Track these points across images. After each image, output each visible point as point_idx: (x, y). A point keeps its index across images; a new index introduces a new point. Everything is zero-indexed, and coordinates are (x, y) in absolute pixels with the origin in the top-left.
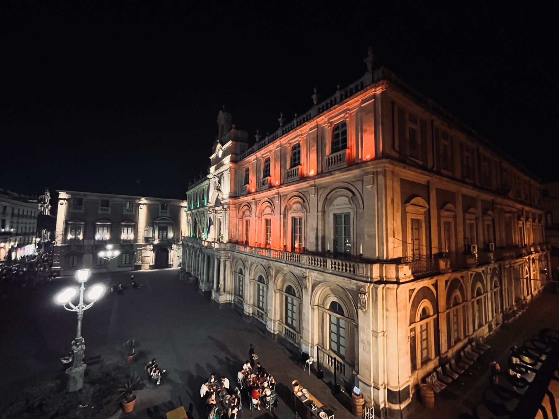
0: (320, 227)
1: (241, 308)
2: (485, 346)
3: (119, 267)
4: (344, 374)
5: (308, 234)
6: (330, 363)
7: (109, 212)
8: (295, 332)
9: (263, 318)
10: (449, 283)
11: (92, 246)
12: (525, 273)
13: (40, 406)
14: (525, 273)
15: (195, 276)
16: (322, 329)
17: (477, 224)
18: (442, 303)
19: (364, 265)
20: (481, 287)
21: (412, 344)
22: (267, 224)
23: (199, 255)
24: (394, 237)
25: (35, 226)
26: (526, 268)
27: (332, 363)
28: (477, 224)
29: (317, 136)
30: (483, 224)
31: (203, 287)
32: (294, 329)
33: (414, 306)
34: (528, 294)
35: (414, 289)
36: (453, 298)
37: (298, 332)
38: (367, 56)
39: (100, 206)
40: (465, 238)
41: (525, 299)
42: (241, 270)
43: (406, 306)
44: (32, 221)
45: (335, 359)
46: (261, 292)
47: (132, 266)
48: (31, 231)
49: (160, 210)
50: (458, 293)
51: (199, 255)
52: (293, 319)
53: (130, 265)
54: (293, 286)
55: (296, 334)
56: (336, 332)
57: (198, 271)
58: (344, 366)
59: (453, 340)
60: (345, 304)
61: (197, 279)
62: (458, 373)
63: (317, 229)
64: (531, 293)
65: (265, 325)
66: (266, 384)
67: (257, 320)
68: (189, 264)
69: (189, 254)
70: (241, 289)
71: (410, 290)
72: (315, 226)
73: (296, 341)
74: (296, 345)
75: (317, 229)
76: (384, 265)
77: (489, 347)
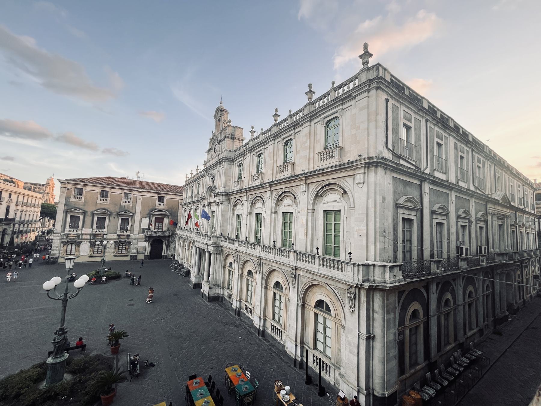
0: (310, 224)
1: (229, 302)
2: (476, 352)
4: (330, 376)
6: (315, 363)
7: (108, 202)
10: (440, 286)
11: (91, 235)
12: (517, 276)
13: (17, 396)
14: (517, 276)
17: (470, 226)
18: (433, 306)
19: (507, 251)
20: (473, 290)
24: (385, 236)
25: (39, 214)
26: (519, 272)
27: (317, 362)
28: (470, 226)
30: (476, 226)
31: (193, 279)
32: (281, 325)
33: (404, 309)
34: (520, 299)
35: (404, 291)
37: (284, 330)
41: (516, 303)
42: (231, 263)
43: (395, 308)
44: (36, 209)
45: (320, 359)
49: (157, 203)
50: (449, 296)
52: (280, 317)
53: (126, 254)
55: (283, 330)
58: (330, 367)
59: (443, 344)
64: (524, 298)
65: (252, 320)
69: (183, 247)
71: (217, 109)
72: (305, 223)
74: (282, 343)
76: (178, 232)
77: (480, 353)
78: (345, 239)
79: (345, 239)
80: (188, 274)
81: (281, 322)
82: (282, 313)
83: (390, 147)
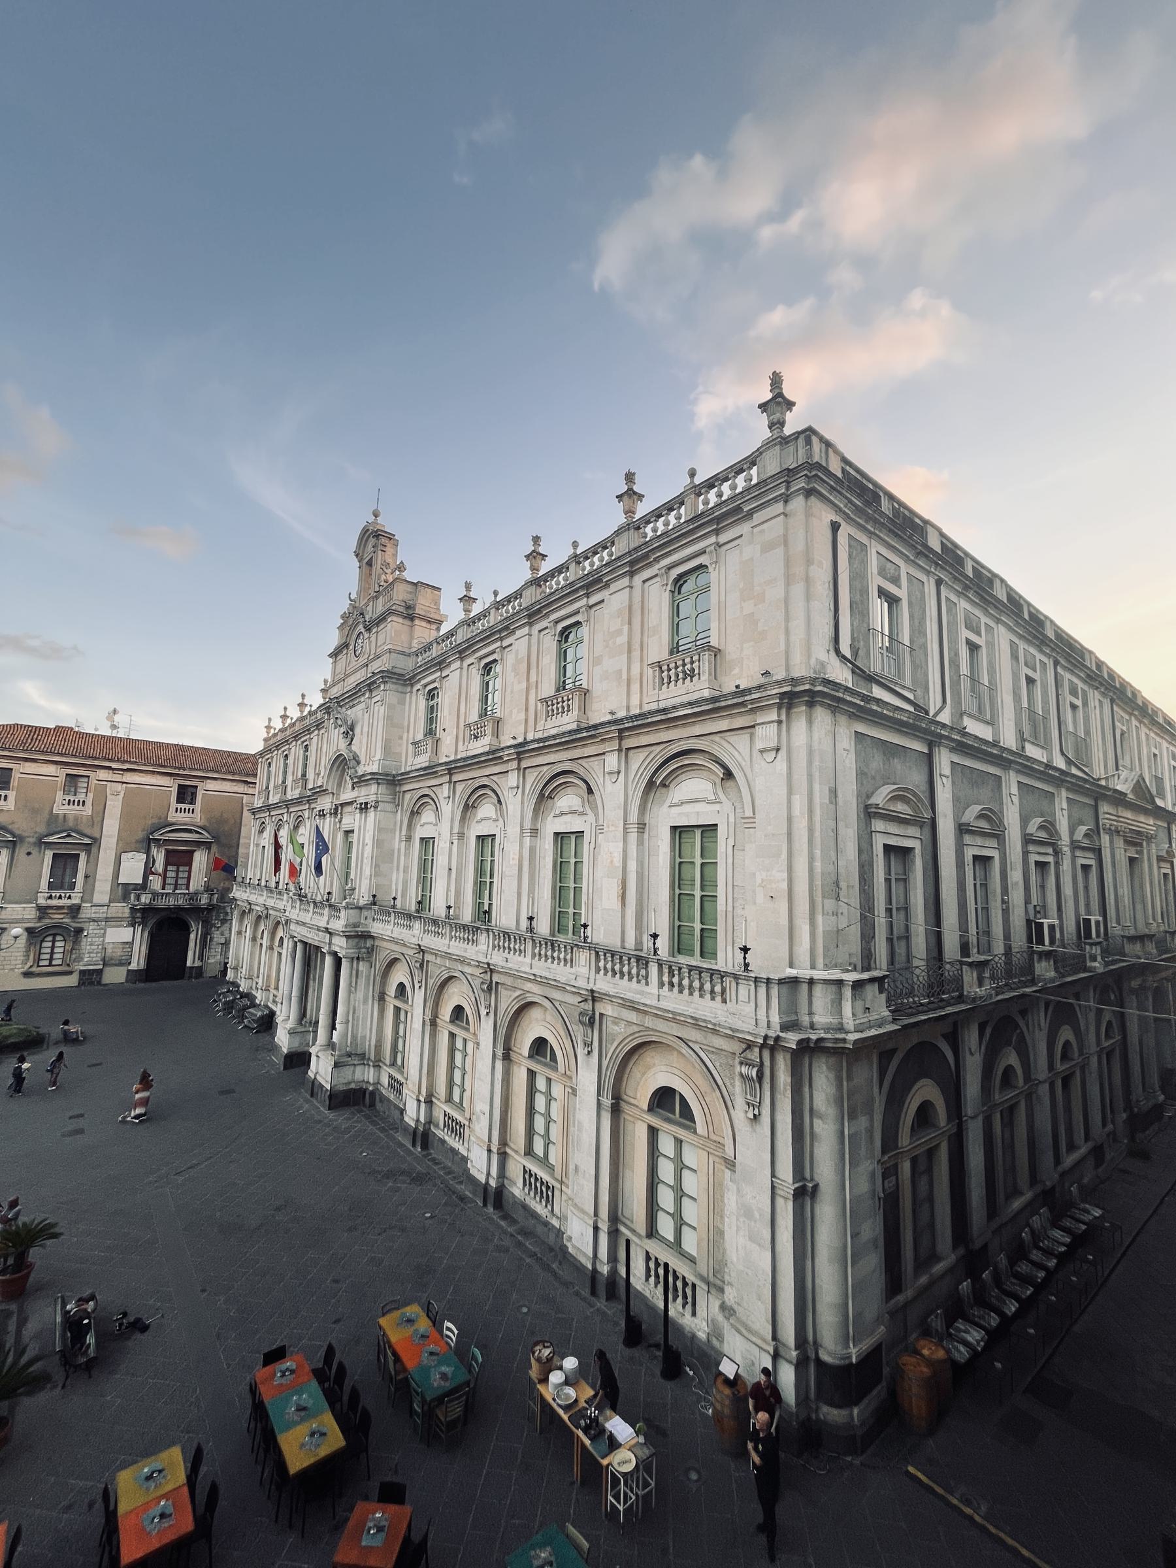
0: (632, 866)
3: (27, 974)
8: (552, 1182)
10: (988, 1031)
15: (266, 1006)
17: (1057, 863)
22: (480, 852)
24: (838, 898)
28: (1057, 863)
31: (283, 1039)
32: (550, 1168)
33: (895, 1102)
36: (1000, 1073)
37: (562, 1182)
38: (531, 1368)
39: (60, 794)
40: (1027, 901)
42: (401, 986)
47: (71, 973)
48: (438, 823)
49: (174, 805)
50: (1011, 1058)
54: (552, 1040)
55: (557, 1185)
57: (277, 988)
58: (694, 1286)
60: (701, 1097)
62: (1016, 1298)
68: (251, 966)
69: (254, 939)
70: (400, 1047)
74: (555, 1222)
77: (1097, 1213)
78: (730, 908)
79: (730, 908)
80: (268, 1022)
81: (552, 1160)
82: (555, 1132)
83: (846, 650)
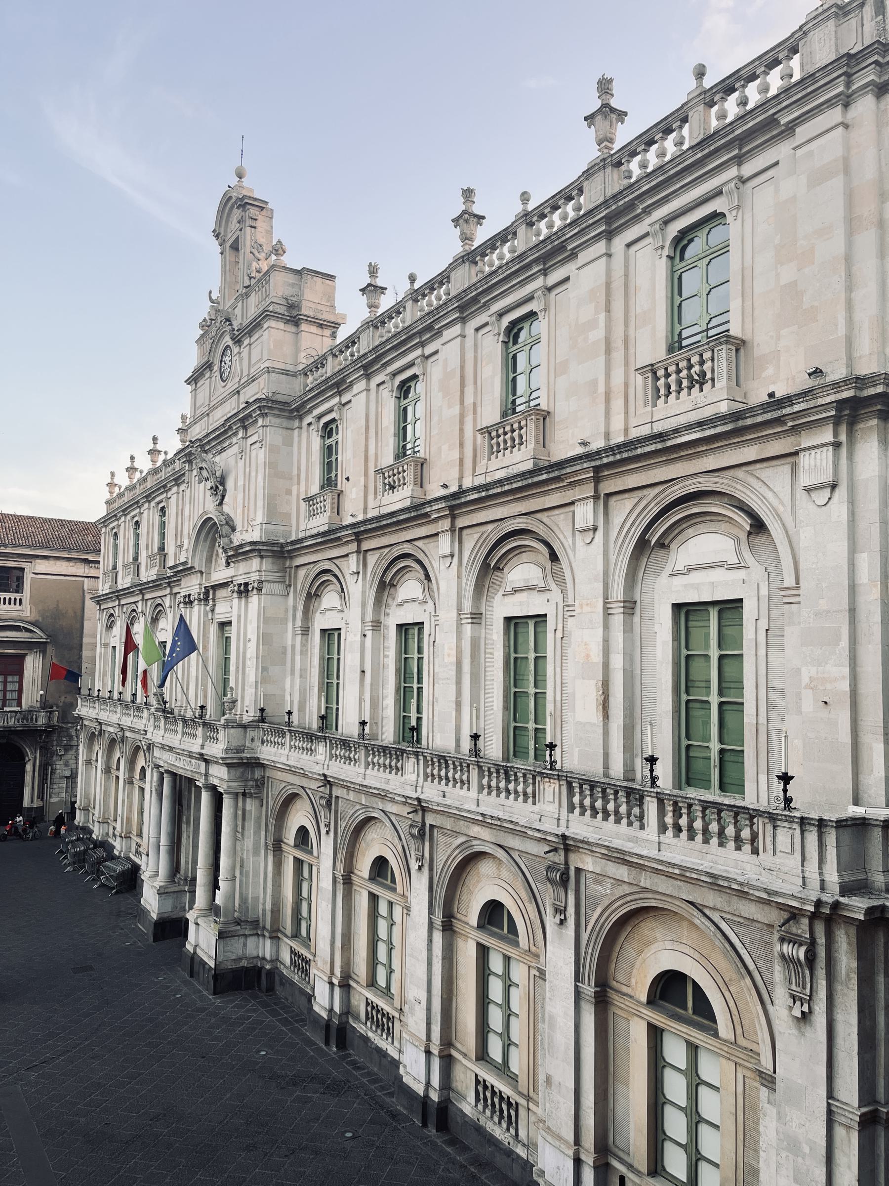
0: (617, 662)
1: (302, 992)
5: (569, 689)
8: (515, 1098)
9: (390, 1032)
15: (128, 859)
16: (783, 525)
21: (506, 726)
23: (143, 769)
29: (608, 285)
32: (513, 1079)
37: (528, 1098)
46: (382, 925)
51: (143, 769)
52: (508, 1045)
55: (522, 1102)
56: (683, 1066)
57: (140, 835)
61: (136, 868)
63: (606, 666)
65: (396, 1064)
66: (822, 688)
67: (366, 1039)
72: (597, 657)
73: (522, 1134)
74: (521, 1151)
75: (606, 666)
